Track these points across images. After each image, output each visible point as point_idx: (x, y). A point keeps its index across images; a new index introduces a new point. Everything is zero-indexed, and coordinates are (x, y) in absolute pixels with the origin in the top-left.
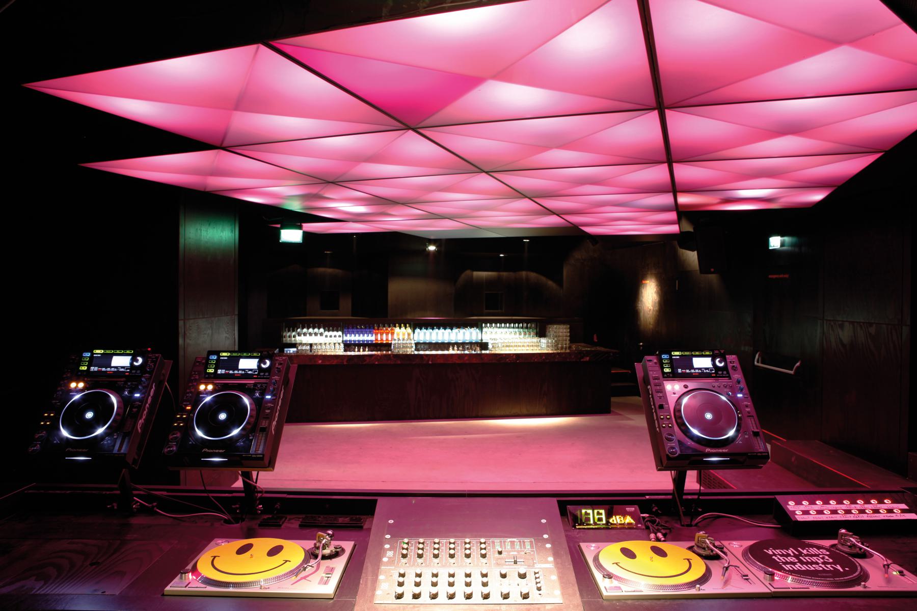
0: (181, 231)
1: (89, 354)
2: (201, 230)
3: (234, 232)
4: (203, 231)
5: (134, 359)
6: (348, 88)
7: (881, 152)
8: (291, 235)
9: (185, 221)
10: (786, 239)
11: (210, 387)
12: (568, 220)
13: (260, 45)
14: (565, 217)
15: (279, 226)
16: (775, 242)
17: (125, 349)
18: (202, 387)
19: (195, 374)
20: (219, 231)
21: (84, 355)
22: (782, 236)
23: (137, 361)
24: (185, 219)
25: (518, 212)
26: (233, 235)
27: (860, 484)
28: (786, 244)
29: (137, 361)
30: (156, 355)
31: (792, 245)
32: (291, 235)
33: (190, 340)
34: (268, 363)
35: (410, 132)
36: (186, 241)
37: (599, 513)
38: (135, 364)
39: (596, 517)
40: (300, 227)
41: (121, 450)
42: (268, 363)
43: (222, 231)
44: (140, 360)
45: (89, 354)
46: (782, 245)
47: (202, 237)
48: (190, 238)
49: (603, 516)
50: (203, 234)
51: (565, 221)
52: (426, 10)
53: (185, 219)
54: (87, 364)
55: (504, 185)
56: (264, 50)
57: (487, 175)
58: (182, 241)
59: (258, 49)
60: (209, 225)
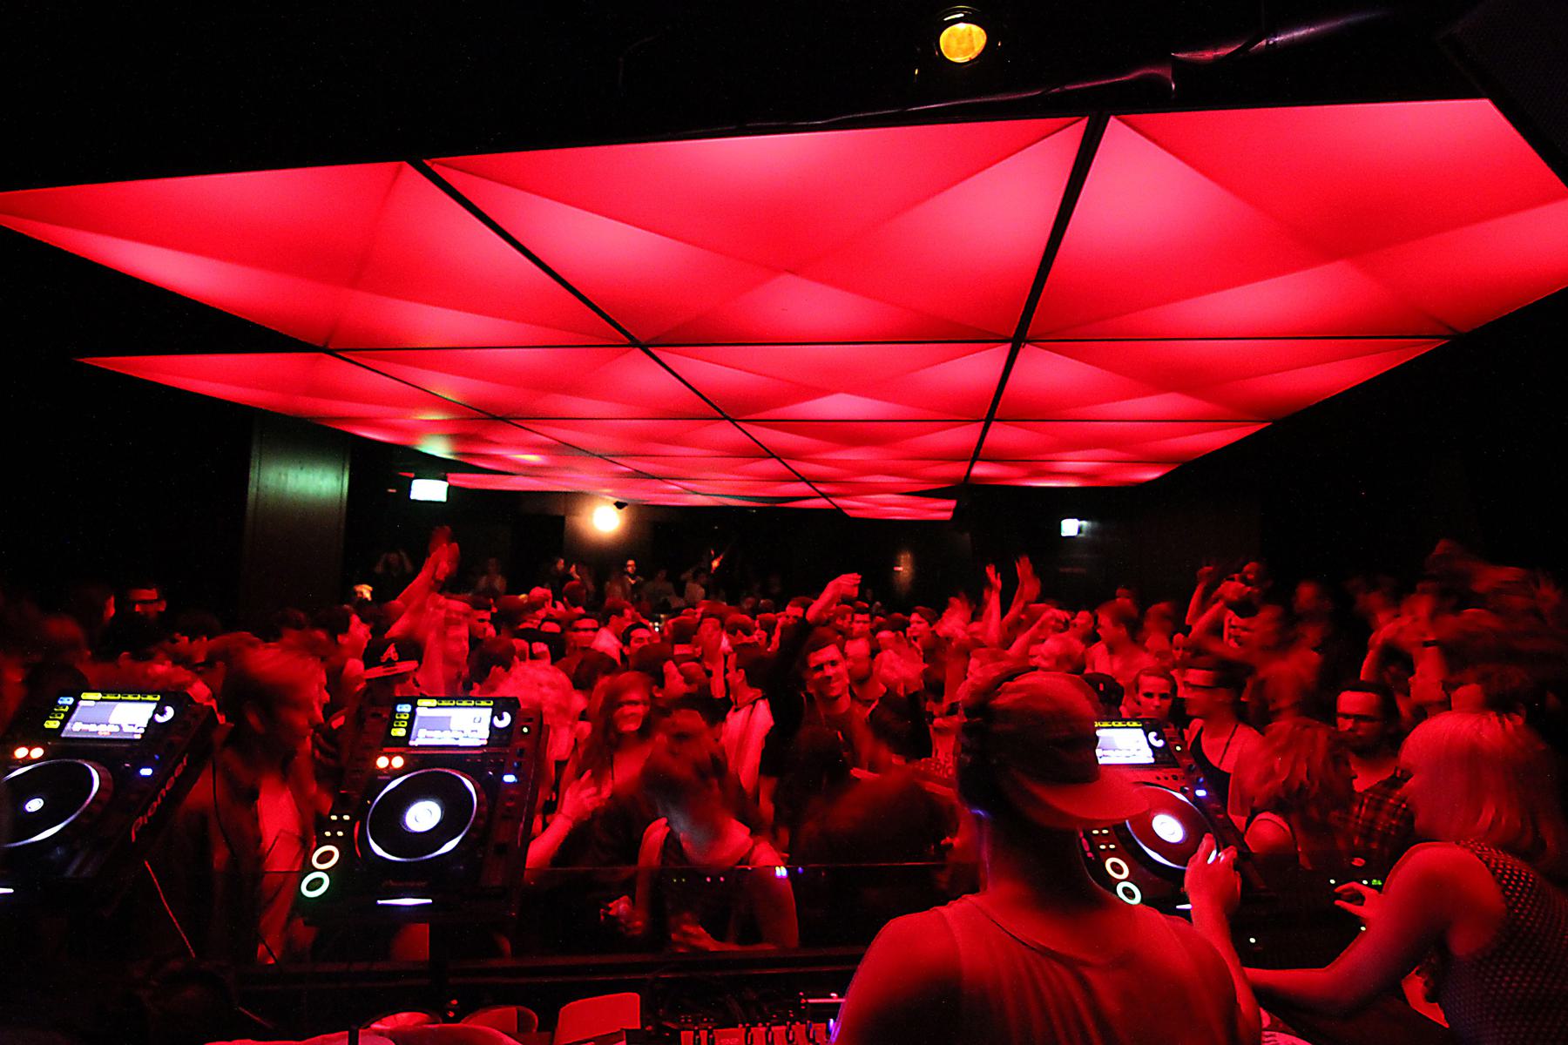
0: (253, 475)
2: (286, 475)
5: (160, 710)
6: (547, 263)
7: (1177, 463)
9: (260, 458)
10: (1084, 523)
12: (793, 468)
13: (405, 164)
14: (833, 500)
16: (1070, 527)
17: (144, 694)
18: (382, 762)
22: (1080, 519)
23: (163, 713)
24: (261, 454)
25: (755, 475)
26: (340, 484)
28: (1084, 529)
29: (163, 713)
31: (1092, 531)
33: (1509, 720)
35: (638, 350)
38: (159, 719)
40: (445, 479)
41: (1166, 694)
42: (507, 717)
44: (170, 712)
46: (1080, 530)
47: (288, 486)
48: (267, 487)
50: (289, 482)
51: (787, 470)
52: (1035, 622)
53: (261, 454)
55: (571, 296)
56: (410, 175)
57: (732, 426)
58: (252, 490)
59: (398, 171)
60: (302, 469)
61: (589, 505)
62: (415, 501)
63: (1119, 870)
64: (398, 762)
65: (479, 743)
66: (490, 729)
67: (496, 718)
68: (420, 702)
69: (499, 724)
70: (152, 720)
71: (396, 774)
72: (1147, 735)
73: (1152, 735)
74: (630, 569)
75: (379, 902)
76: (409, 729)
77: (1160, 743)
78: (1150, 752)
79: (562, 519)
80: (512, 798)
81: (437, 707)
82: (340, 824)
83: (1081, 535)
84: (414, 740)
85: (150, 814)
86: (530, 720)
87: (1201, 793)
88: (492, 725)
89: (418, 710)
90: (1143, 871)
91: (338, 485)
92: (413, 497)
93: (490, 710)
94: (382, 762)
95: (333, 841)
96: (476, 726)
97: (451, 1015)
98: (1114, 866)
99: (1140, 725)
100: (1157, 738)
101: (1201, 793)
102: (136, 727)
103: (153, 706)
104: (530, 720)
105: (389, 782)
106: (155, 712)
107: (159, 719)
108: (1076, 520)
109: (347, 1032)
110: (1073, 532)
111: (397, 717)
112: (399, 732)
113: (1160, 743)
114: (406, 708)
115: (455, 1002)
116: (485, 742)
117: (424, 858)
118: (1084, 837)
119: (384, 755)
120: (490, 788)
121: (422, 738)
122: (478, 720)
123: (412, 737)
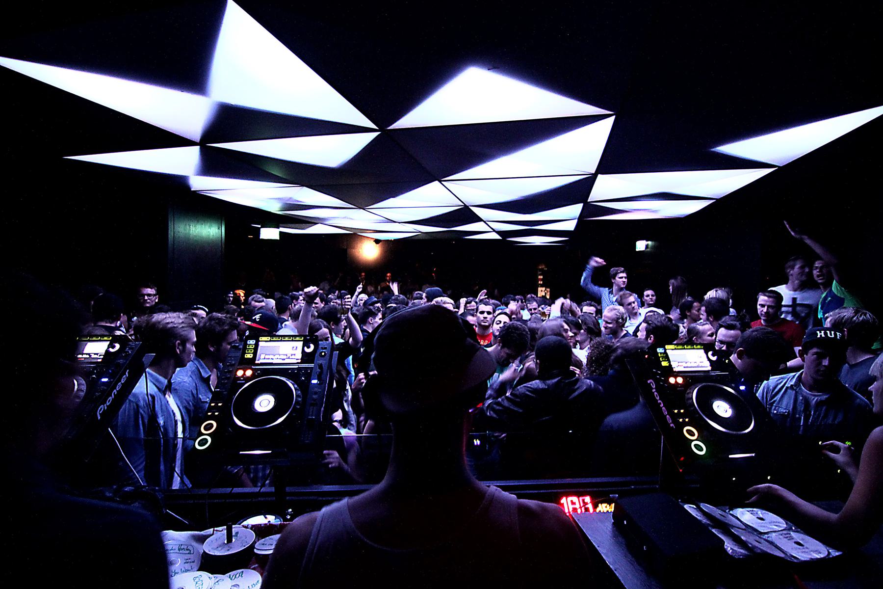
1: (254, 341)
3: (220, 229)
4: (191, 226)
5: (112, 345)
8: (269, 234)
10: (650, 243)
11: (249, 373)
15: (260, 226)
16: (641, 245)
18: (240, 373)
19: (231, 360)
20: (207, 227)
21: (248, 343)
23: (113, 347)
26: (220, 231)
27: (174, 461)
29: (113, 347)
30: (130, 337)
31: (653, 247)
32: (269, 234)
34: (312, 346)
36: (175, 235)
37: (573, 503)
38: (111, 350)
39: (571, 507)
42: (312, 346)
43: (210, 227)
45: (254, 341)
46: (647, 246)
49: (590, 506)
54: (252, 352)
58: (171, 234)
60: (198, 222)
61: (360, 242)
62: (263, 240)
63: (692, 434)
64: (249, 373)
65: (296, 361)
66: (302, 353)
67: (306, 348)
68: (261, 339)
69: (307, 350)
70: (107, 351)
71: (248, 379)
72: (707, 353)
73: (710, 353)
74: (388, 278)
75: (109, 429)
76: (255, 354)
77: (714, 358)
78: (708, 363)
79: (346, 250)
80: (316, 393)
81: (270, 341)
82: (216, 408)
83: (648, 250)
84: (259, 360)
85: (108, 404)
86: (325, 348)
87: (742, 388)
88: (303, 351)
89: (260, 343)
90: (707, 434)
91: (219, 232)
92: (261, 237)
93: (302, 342)
94: (240, 373)
95: (212, 418)
96: (293, 352)
97: (289, 517)
98: (689, 432)
99: (702, 347)
100: (713, 355)
101: (742, 388)
102: (99, 355)
103: (108, 343)
104: (325, 348)
105: (244, 384)
106: (108, 348)
107: (111, 350)
108: (645, 241)
109: (225, 527)
110: (643, 248)
111: (248, 347)
112: (249, 356)
113: (714, 358)
114: (252, 342)
115: (290, 510)
116: (299, 361)
117: (265, 427)
118: (668, 414)
119: (240, 369)
120: (304, 386)
121: (262, 359)
122: (295, 348)
123: (257, 359)
